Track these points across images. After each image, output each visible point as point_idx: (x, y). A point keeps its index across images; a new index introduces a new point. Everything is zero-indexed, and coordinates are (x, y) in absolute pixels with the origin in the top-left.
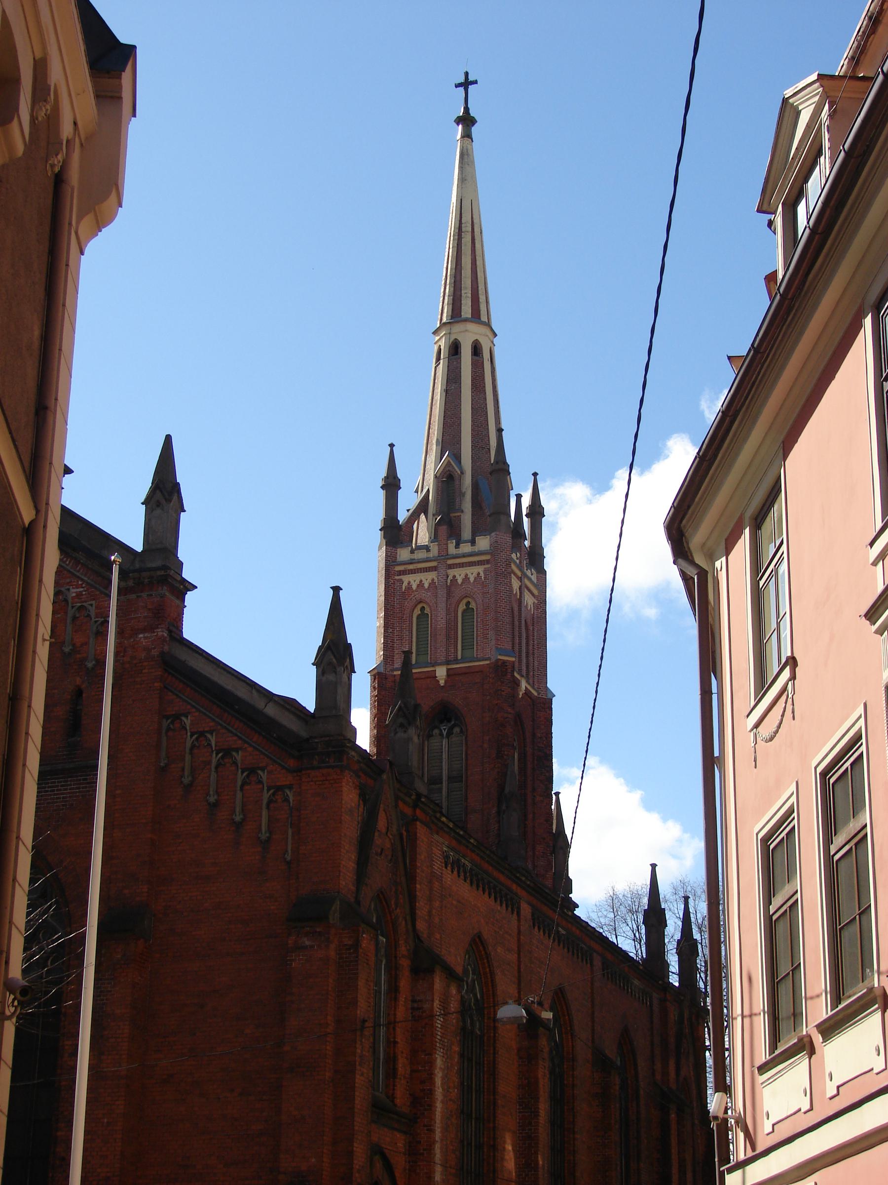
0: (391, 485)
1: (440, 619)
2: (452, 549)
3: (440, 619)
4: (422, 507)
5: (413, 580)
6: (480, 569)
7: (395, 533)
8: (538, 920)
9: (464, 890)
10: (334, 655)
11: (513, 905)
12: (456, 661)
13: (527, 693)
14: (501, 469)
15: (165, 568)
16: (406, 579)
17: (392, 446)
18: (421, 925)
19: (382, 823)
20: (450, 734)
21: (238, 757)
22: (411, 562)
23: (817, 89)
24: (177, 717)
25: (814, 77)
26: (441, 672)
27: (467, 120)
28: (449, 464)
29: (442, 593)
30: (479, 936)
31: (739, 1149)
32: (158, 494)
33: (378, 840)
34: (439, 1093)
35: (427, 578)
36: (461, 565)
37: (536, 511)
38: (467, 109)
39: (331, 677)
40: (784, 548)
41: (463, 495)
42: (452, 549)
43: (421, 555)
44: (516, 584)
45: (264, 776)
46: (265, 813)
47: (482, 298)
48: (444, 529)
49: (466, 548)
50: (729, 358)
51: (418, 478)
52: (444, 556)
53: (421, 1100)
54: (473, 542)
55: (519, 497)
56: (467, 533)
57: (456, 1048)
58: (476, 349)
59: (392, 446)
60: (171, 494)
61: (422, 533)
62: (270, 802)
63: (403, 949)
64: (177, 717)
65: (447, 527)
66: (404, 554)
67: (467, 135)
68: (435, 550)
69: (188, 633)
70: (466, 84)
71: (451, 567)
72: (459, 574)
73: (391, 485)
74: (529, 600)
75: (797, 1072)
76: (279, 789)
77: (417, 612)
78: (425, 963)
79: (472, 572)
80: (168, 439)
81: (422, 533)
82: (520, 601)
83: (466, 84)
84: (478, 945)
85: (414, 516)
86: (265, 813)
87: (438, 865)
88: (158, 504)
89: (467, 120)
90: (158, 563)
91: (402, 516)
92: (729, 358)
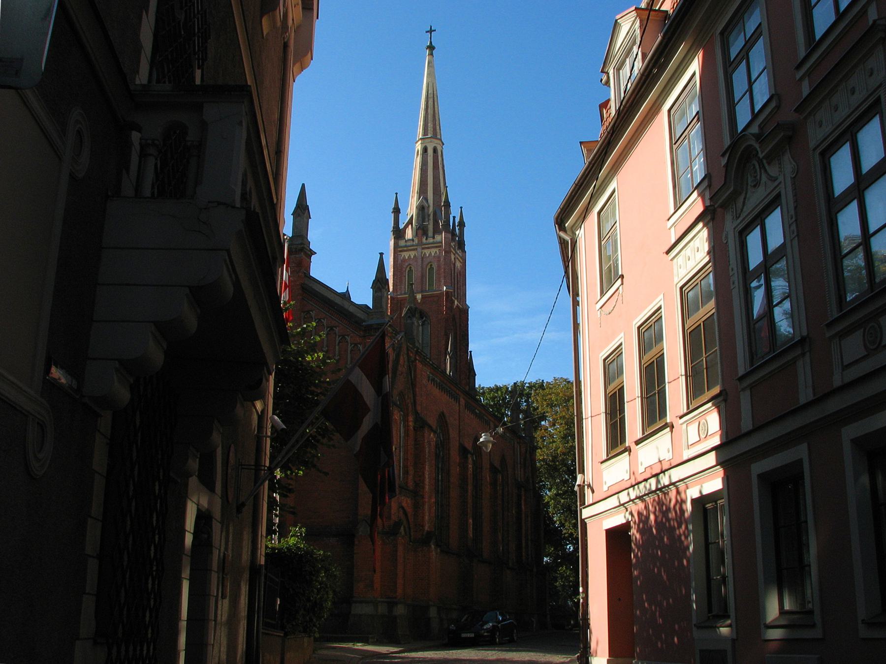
0: (397, 211)
1: (416, 274)
2: (424, 240)
3: (435, 266)
4: (410, 222)
5: (406, 255)
6: (437, 250)
7: (398, 233)
8: (467, 406)
9: (436, 391)
10: (380, 283)
11: (457, 400)
12: (426, 291)
13: (457, 306)
14: (447, 204)
15: (302, 244)
16: (403, 254)
17: (381, 254)
18: (419, 408)
19: (401, 361)
20: (423, 325)
21: (337, 330)
22: (406, 246)
23: (634, 14)
24: (308, 312)
25: (633, 8)
26: (419, 296)
27: (431, 48)
28: (422, 201)
29: (420, 261)
30: (443, 413)
31: (589, 498)
32: (299, 211)
33: (400, 368)
34: (427, 481)
35: (412, 254)
36: (428, 248)
37: (462, 224)
38: (431, 42)
39: (379, 294)
40: (618, 223)
41: (429, 216)
42: (424, 240)
43: (409, 244)
44: (453, 257)
45: (348, 339)
46: (349, 356)
47: (438, 128)
48: (420, 232)
49: (431, 240)
50: (581, 143)
51: (410, 209)
52: (420, 243)
53: (419, 484)
54: (434, 238)
55: (454, 217)
56: (430, 233)
57: (433, 462)
58: (435, 150)
59: (381, 254)
60: (305, 210)
61: (409, 234)
62: (352, 351)
63: (411, 419)
64: (308, 312)
65: (421, 230)
66: (402, 243)
67: (431, 54)
68: (416, 241)
69: (313, 274)
70: (431, 31)
71: (423, 249)
72: (427, 252)
73: (397, 211)
74: (458, 264)
75: (663, 440)
76: (356, 345)
77: (408, 269)
78: (421, 424)
79: (433, 251)
80: (303, 185)
81: (409, 234)
82: (454, 265)
83: (431, 31)
84: (442, 416)
85: (406, 226)
86: (349, 356)
87: (425, 381)
88: (299, 215)
89: (431, 48)
90: (300, 242)
91: (401, 226)
92: (581, 143)
